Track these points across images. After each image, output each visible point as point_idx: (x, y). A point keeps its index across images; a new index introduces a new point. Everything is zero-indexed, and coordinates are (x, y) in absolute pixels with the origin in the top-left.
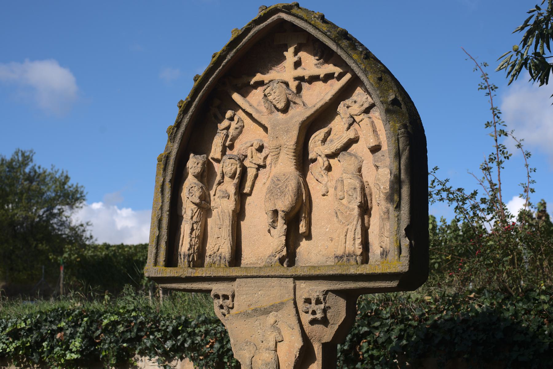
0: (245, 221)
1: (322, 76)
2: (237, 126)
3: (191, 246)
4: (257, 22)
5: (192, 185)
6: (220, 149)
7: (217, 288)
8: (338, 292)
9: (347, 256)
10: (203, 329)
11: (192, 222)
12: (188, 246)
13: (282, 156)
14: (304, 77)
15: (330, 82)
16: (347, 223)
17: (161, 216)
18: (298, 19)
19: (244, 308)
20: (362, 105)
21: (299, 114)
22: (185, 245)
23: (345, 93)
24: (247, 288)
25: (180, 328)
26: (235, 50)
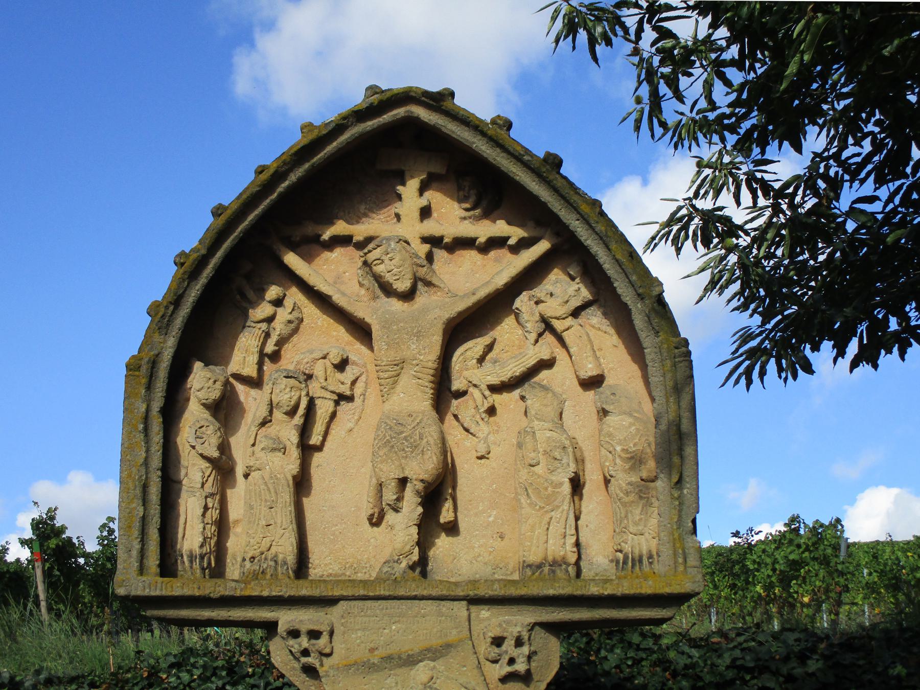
0: (312, 498)
1: (482, 240)
2: (290, 317)
3: (205, 539)
4: (359, 115)
5: (202, 423)
6: (254, 358)
7: (286, 618)
8: (552, 628)
9: (550, 565)
11: (204, 495)
12: (201, 539)
13: (406, 380)
15: (493, 254)
16: (548, 508)
17: (147, 478)
18: (455, 123)
19: (361, 653)
20: (567, 301)
22: (192, 536)
24: (365, 619)
26: (307, 166)
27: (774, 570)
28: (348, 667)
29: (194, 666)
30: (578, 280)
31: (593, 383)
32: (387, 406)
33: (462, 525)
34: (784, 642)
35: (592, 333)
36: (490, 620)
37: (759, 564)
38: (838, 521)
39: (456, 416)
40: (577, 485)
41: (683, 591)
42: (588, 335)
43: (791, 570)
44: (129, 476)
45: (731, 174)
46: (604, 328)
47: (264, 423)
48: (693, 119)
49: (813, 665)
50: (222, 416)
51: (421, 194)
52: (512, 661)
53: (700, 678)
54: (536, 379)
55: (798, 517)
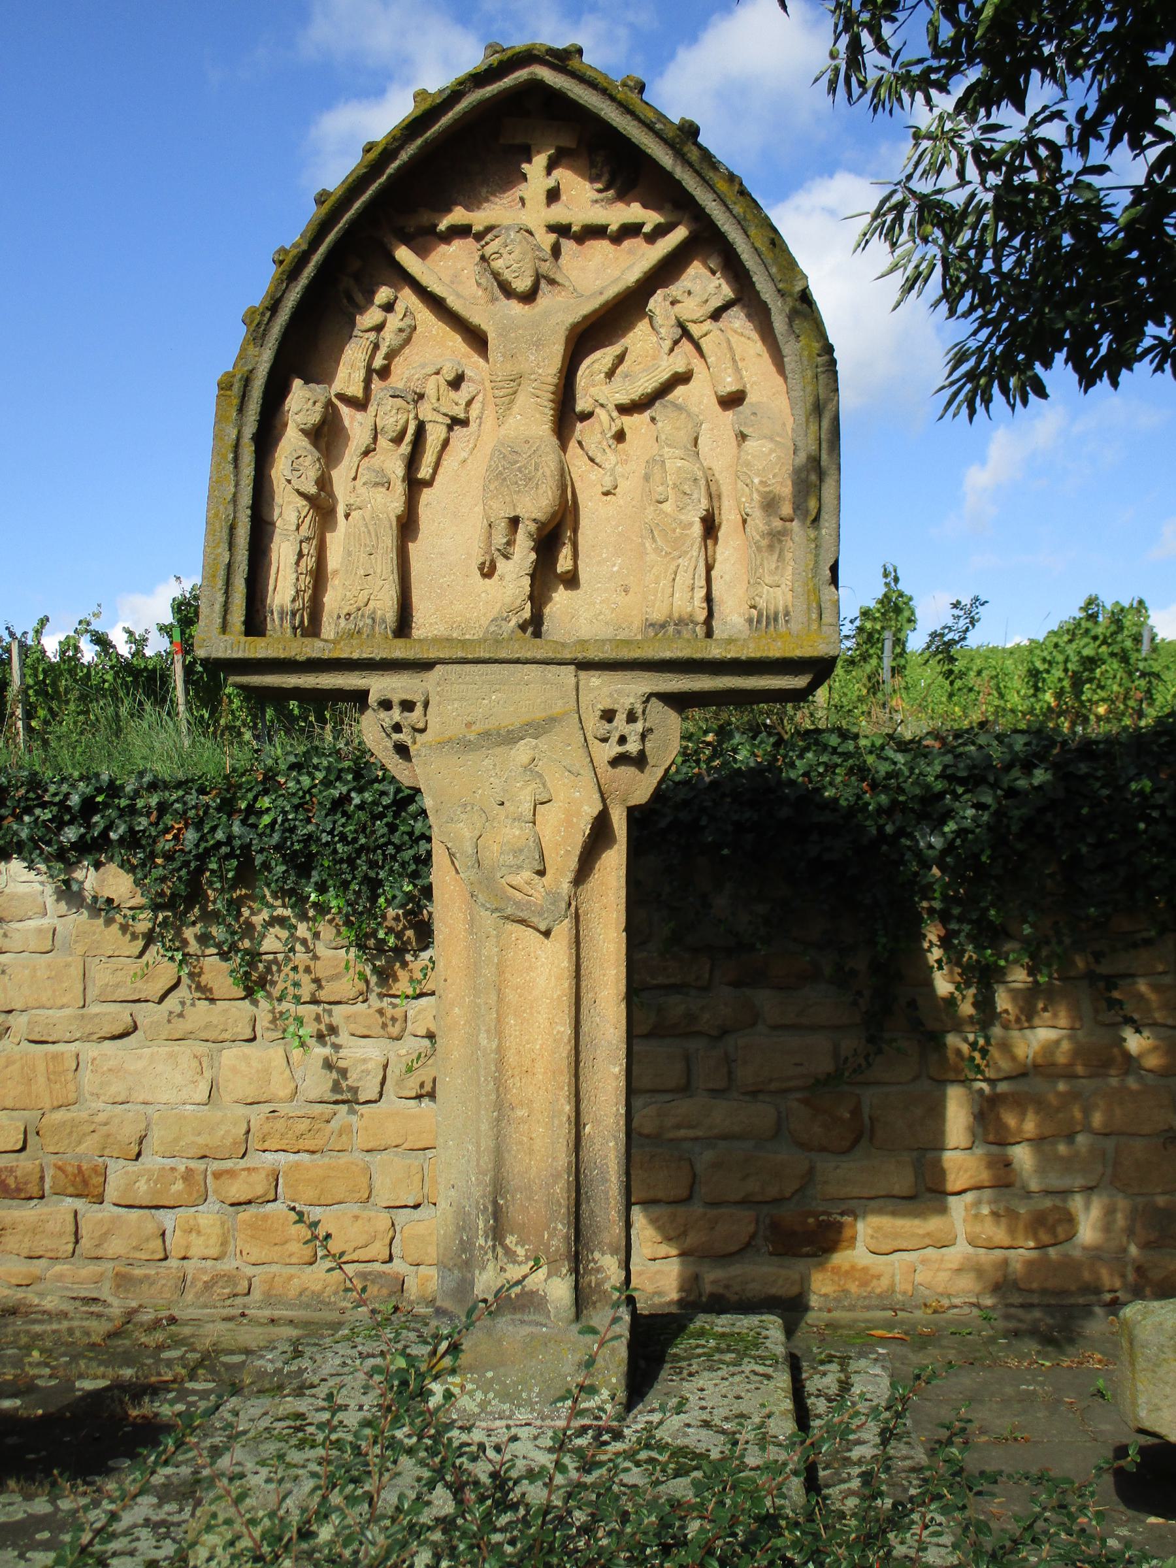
1: (614, 227)
2: (401, 325)
4: (478, 79)
6: (361, 374)
7: (378, 685)
8: (669, 699)
10: (154, 801)
12: (293, 593)
13: (523, 399)
14: (569, 226)
15: (627, 244)
16: (676, 553)
18: (583, 86)
19: (456, 729)
21: (561, 310)
22: (283, 589)
23: (665, 272)
25: (99, 799)
26: (419, 141)
27: (1066, 670)
28: (442, 744)
29: (316, 768)
30: (718, 275)
31: (732, 401)
32: (503, 431)
33: (583, 576)
34: (1010, 746)
35: (734, 339)
36: (603, 689)
37: (1050, 663)
38: (1141, 602)
39: (580, 443)
40: (710, 527)
41: (815, 654)
42: (729, 342)
43: (1085, 670)
44: (216, 515)
45: (953, 144)
46: (747, 332)
47: (366, 453)
48: (895, 74)
49: (1040, 776)
50: (323, 445)
51: (549, 173)
52: (622, 740)
53: (900, 790)
54: (670, 397)
55: (1097, 598)
